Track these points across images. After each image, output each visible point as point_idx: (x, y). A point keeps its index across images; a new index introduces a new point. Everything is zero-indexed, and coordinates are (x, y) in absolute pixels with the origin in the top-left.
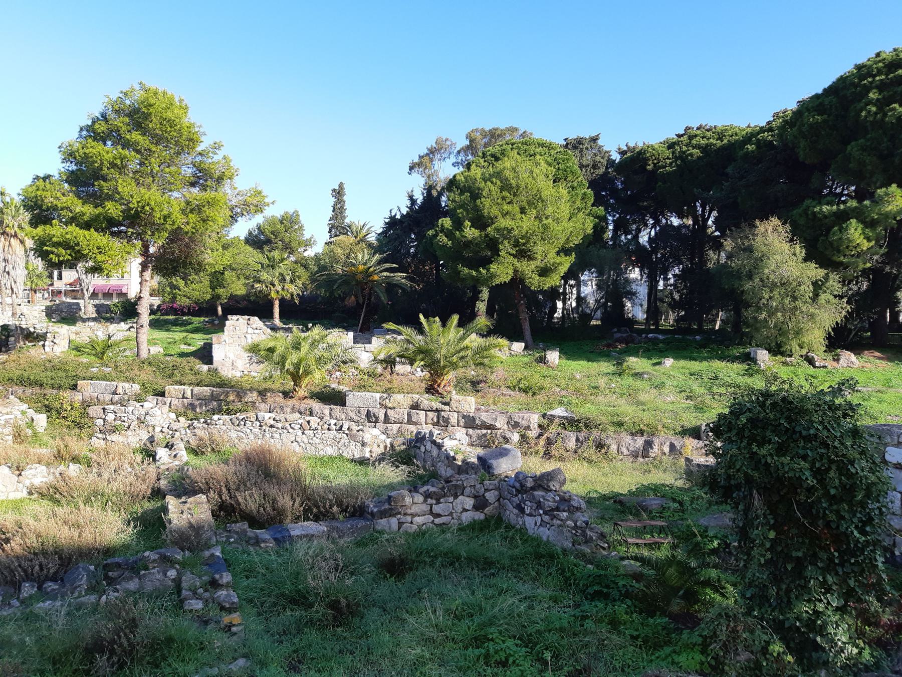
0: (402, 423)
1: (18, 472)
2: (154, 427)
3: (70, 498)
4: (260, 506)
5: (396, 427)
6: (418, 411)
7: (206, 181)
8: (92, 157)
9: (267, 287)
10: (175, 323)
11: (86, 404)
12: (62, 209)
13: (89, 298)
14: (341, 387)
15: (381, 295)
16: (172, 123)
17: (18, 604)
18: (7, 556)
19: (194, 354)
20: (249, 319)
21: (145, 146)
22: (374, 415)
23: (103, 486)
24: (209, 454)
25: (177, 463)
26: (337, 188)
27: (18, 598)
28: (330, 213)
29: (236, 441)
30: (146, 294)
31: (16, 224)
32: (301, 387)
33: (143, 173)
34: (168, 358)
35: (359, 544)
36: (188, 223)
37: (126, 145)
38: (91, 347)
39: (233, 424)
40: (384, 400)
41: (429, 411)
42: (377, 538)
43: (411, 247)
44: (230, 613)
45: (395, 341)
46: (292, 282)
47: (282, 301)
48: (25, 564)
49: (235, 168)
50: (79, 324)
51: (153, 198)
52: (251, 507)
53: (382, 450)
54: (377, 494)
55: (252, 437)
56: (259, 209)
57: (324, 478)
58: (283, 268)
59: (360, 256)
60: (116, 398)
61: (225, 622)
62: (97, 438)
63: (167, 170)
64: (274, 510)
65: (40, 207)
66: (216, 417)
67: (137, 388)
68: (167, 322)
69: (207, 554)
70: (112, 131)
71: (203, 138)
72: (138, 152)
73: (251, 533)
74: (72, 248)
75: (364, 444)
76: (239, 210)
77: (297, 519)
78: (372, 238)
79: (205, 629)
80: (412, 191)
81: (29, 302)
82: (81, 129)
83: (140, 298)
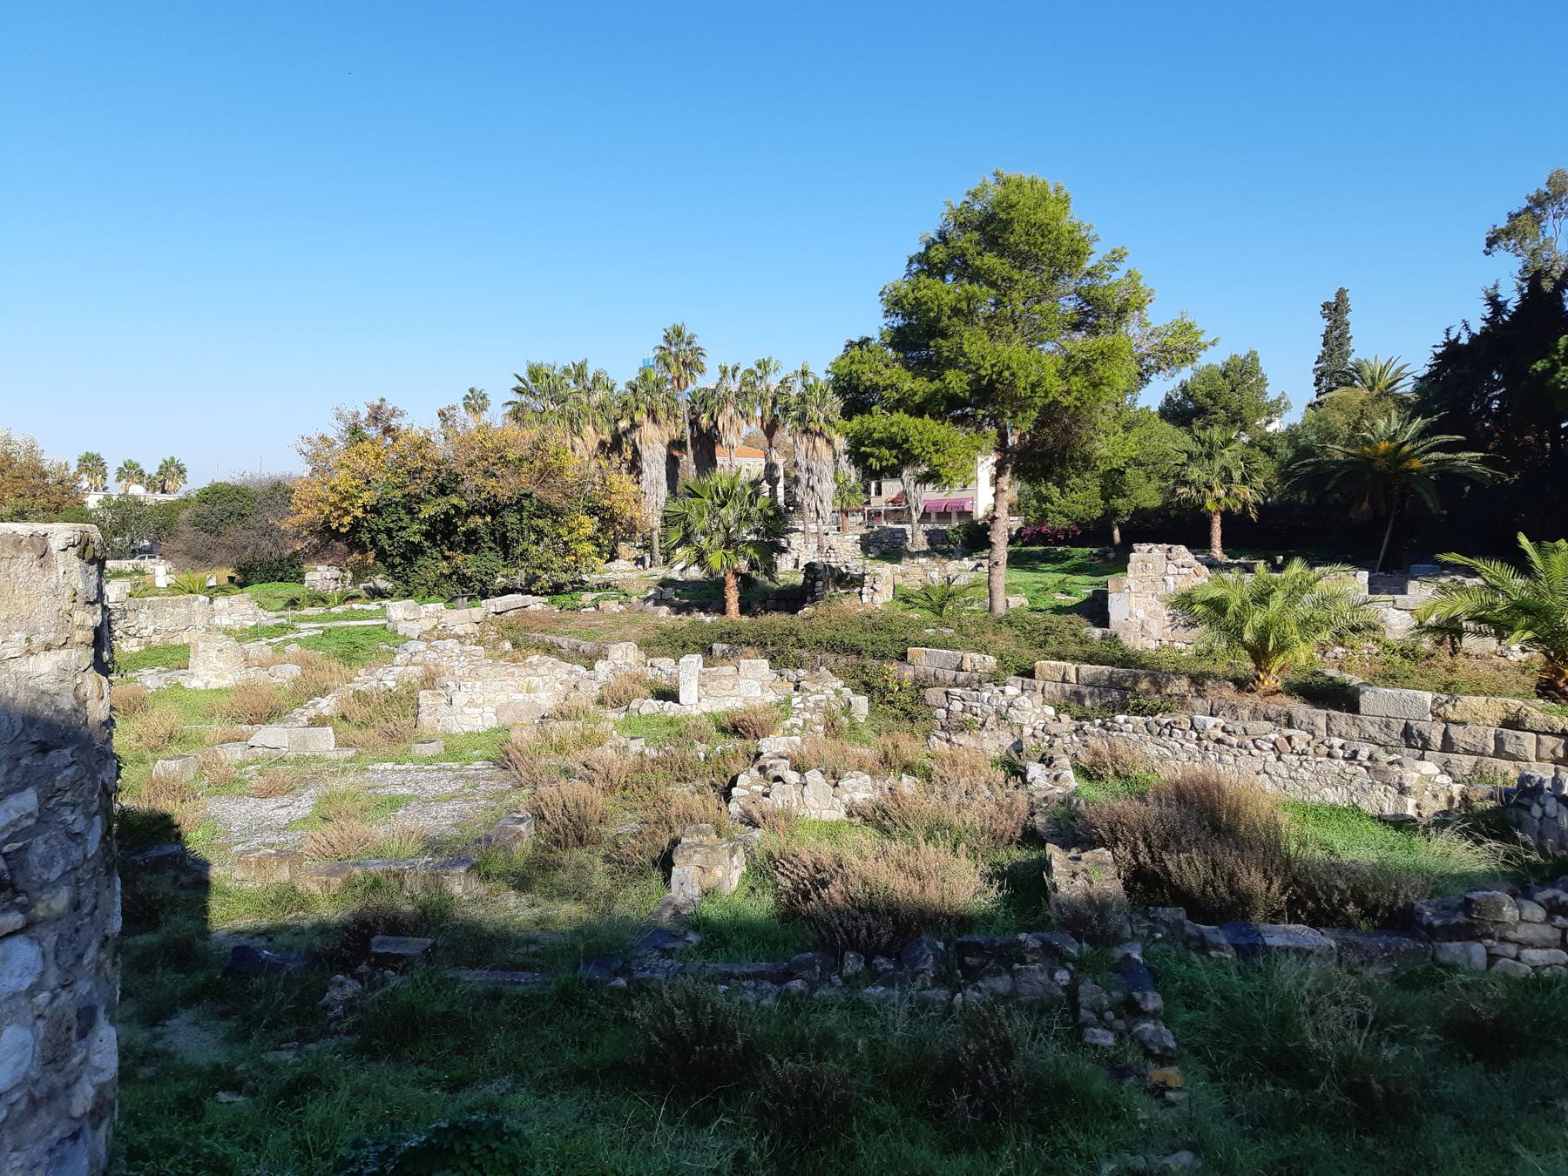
0: (1482, 754)
1: (833, 781)
2: (1021, 727)
3: (904, 829)
4: (1206, 883)
5: (1468, 762)
6: (1519, 733)
7: (1098, 318)
8: (926, 303)
9: (1199, 492)
10: (1045, 558)
11: (921, 685)
12: (885, 389)
13: (919, 522)
14: (1347, 677)
15: (1427, 497)
16: (1044, 230)
17: (839, 982)
18: (825, 906)
19: (1078, 609)
20: (1170, 550)
21: (1004, 273)
22: (1420, 734)
23: (950, 815)
24: (1111, 781)
25: (1059, 790)
26: (1333, 299)
27: (840, 974)
28: (1319, 349)
29: (1156, 762)
30: (1002, 513)
31: (822, 416)
32: (1269, 673)
33: (1000, 319)
34: (1038, 616)
35: (1405, 982)
36: (1069, 392)
37: (976, 276)
38: (924, 596)
39: (1150, 732)
40: (1441, 705)
41: (1546, 733)
42: (1443, 978)
43: (1491, 400)
44: (1163, 1065)
45: (1461, 588)
46: (1244, 480)
47: (1227, 515)
48: (849, 924)
49: (1148, 289)
50: (906, 561)
51: (1015, 356)
52: (1190, 883)
53: (1442, 805)
54: (1436, 892)
55: (1184, 757)
56: (1188, 356)
57: (1324, 846)
58: (1228, 457)
59: (1382, 424)
60: (962, 676)
61: (1155, 1079)
62: (939, 738)
63: (1037, 308)
64: (1232, 893)
65: (856, 389)
66: (1121, 718)
67: (991, 661)
68: (1032, 556)
69: (1118, 953)
70: (954, 257)
71: (1093, 248)
72: (993, 285)
73: (1191, 928)
74: (898, 446)
75: (1403, 790)
76: (1153, 362)
77: (1274, 917)
78: (1406, 388)
79: (1121, 1084)
80: (1496, 287)
81: (839, 529)
82: (911, 262)
83: (994, 518)
